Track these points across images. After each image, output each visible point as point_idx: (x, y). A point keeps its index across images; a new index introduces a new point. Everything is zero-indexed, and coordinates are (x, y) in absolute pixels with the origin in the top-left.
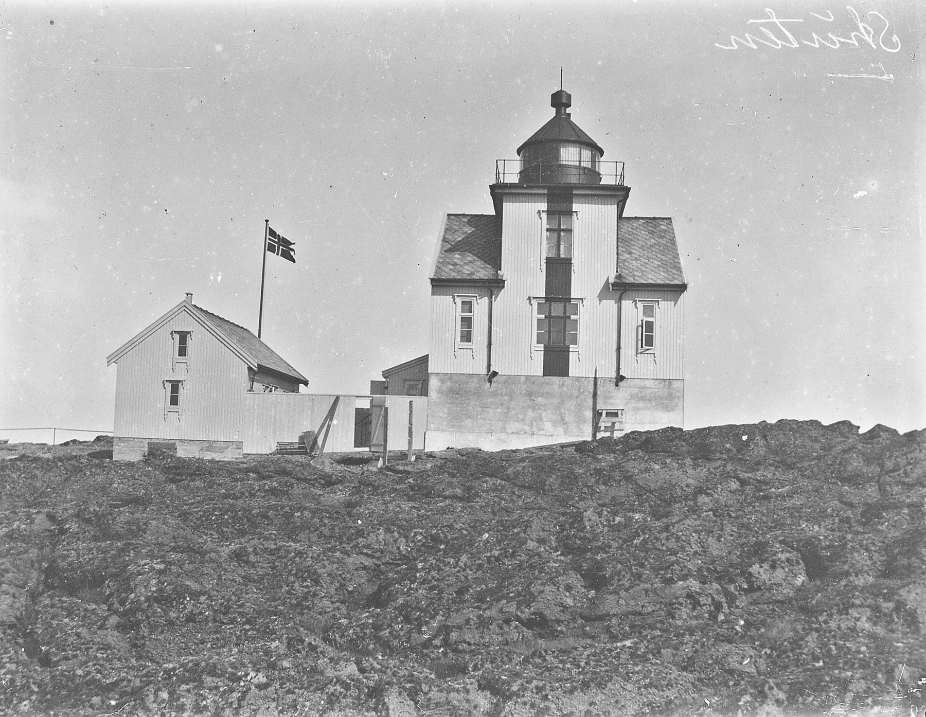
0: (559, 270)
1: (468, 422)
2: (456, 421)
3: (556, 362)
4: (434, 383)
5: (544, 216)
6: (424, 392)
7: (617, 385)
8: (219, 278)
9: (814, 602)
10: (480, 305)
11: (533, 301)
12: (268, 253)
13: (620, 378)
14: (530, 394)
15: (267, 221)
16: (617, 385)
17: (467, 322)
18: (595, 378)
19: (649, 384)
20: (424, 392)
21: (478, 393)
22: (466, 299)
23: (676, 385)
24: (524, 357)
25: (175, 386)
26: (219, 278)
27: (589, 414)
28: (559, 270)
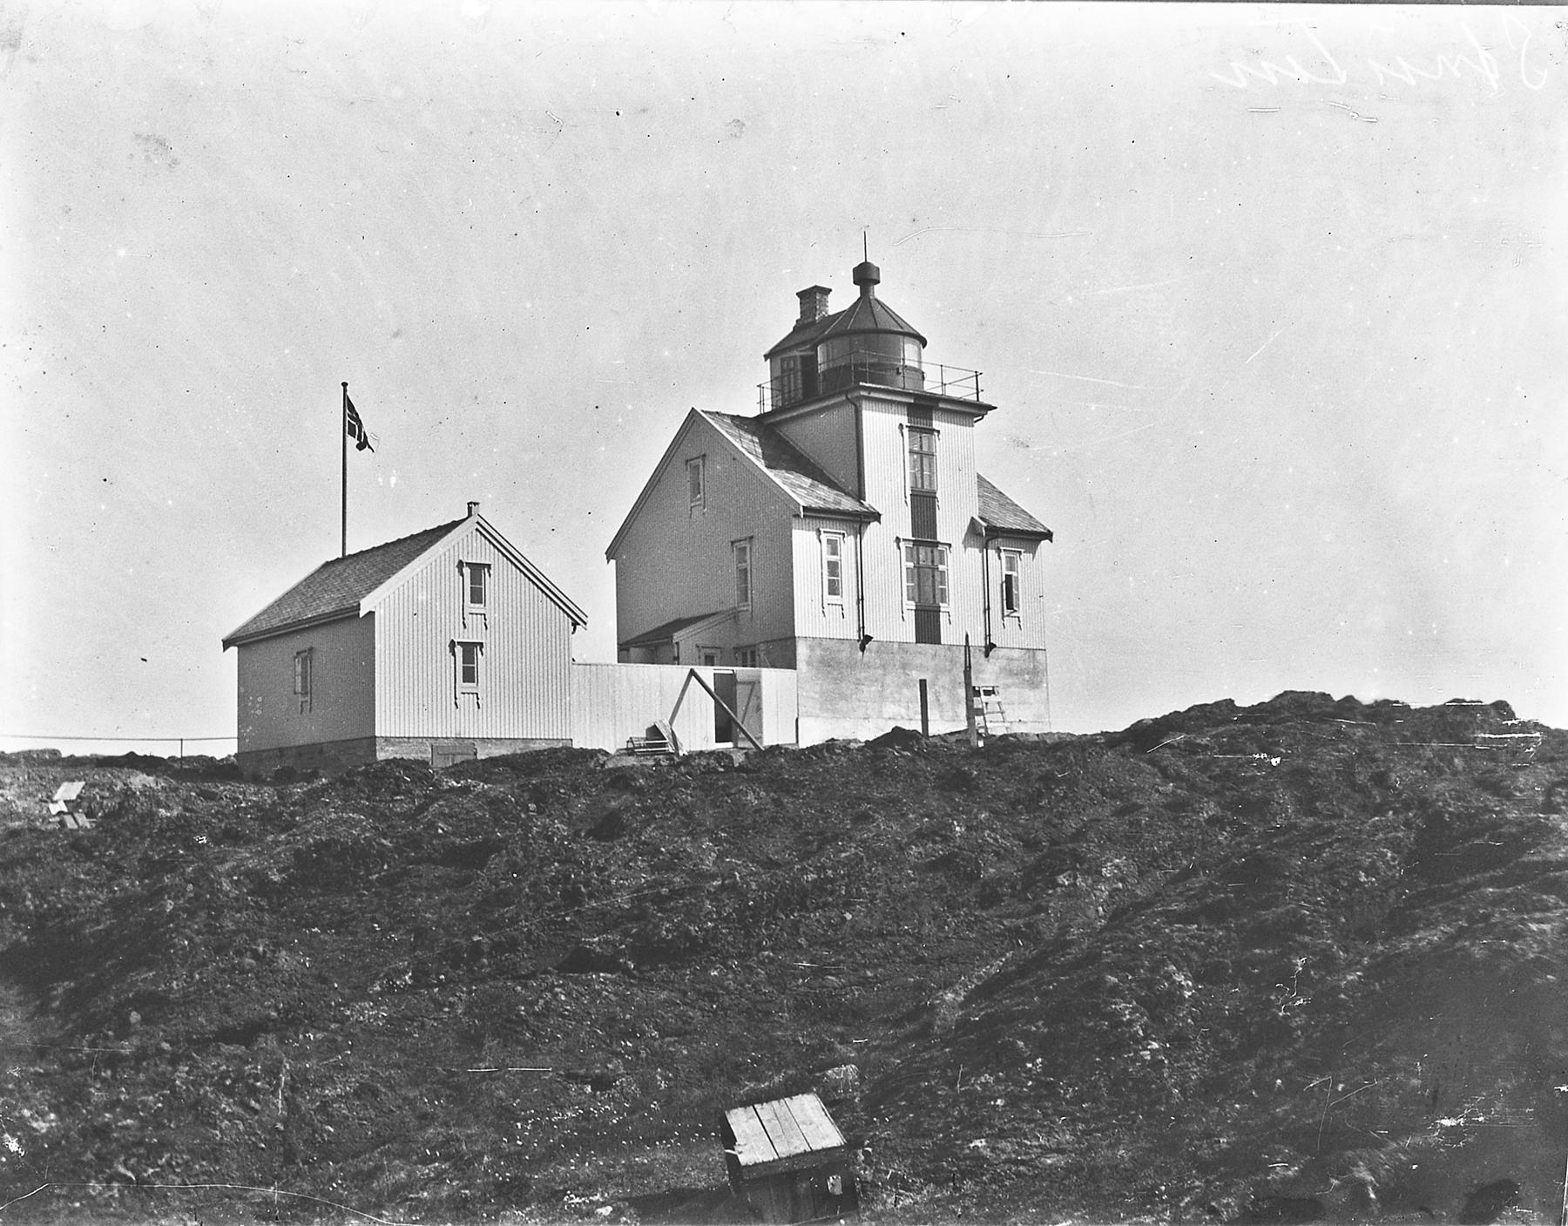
0: (923, 504)
1: (842, 705)
2: (830, 703)
3: (928, 626)
4: (802, 651)
5: (906, 431)
6: (791, 664)
7: (987, 655)
8: (393, 480)
9: (1534, 927)
10: (848, 544)
11: (902, 544)
12: (349, 438)
13: (990, 647)
14: (904, 666)
15: (345, 385)
16: (987, 655)
17: (833, 568)
18: (967, 645)
19: (1016, 654)
20: (791, 664)
21: (852, 666)
22: (833, 537)
23: (1039, 655)
24: (893, 621)
25: (470, 649)
26: (393, 480)
27: (962, 692)
28: (923, 504)
